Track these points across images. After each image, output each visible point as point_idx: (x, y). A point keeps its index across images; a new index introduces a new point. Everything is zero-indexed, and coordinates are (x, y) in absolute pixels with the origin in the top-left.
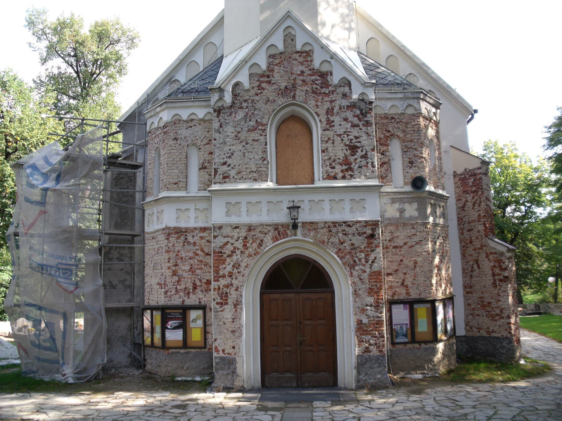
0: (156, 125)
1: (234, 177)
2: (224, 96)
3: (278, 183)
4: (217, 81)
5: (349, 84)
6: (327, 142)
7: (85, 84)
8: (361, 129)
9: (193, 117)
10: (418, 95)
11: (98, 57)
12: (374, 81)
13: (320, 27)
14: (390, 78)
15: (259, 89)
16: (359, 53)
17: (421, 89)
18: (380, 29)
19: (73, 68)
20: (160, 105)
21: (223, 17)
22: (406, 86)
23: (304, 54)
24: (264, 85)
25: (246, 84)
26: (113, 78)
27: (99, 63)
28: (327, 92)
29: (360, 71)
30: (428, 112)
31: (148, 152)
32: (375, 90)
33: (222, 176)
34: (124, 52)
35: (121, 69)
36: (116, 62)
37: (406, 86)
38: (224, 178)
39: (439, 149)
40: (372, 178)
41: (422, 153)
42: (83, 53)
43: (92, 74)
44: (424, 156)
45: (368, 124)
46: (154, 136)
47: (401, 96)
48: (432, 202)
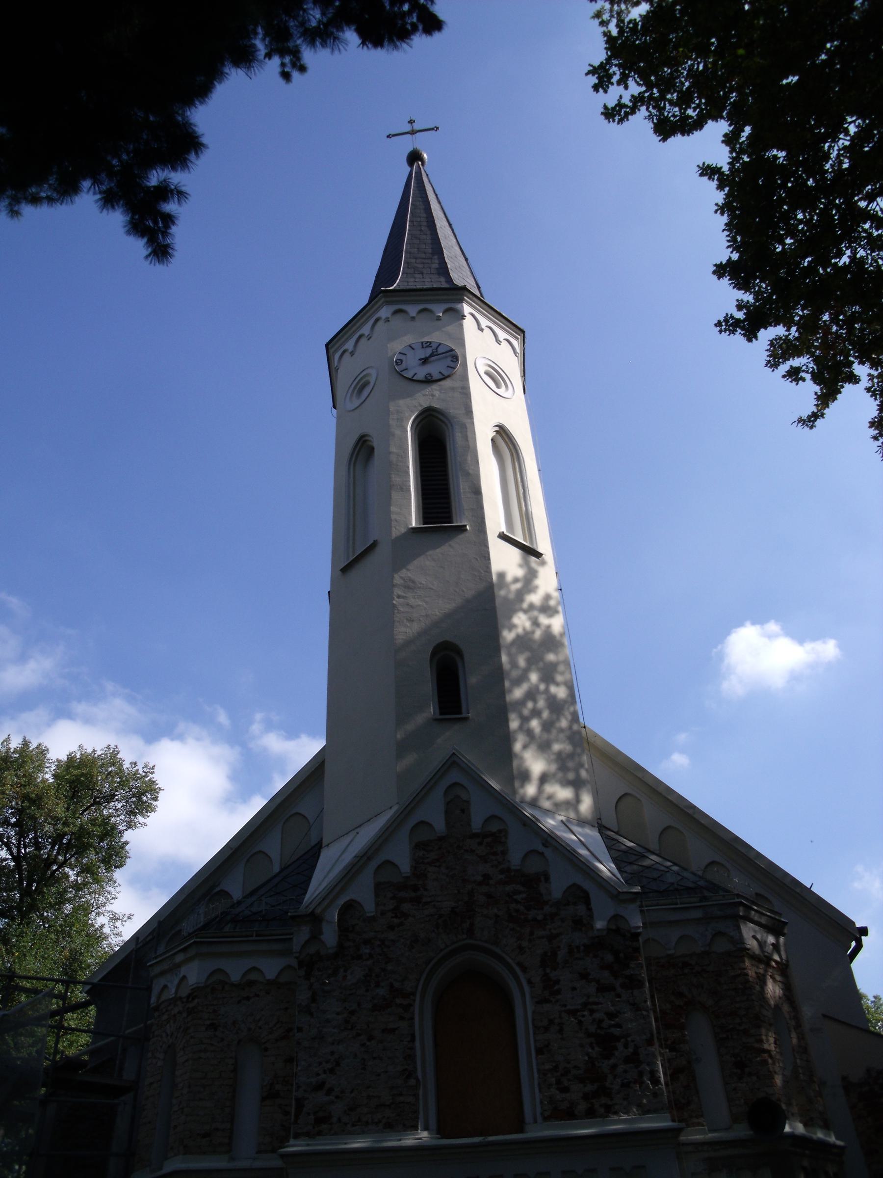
0: (171, 992)
1: (339, 1120)
2: (321, 933)
3: (441, 1131)
4: (308, 897)
5: (585, 898)
6: (546, 1029)
7: (30, 885)
8: (619, 996)
9: (253, 976)
10: (734, 911)
11: (66, 829)
12: (638, 889)
13: (517, 784)
14: (670, 878)
15: (396, 917)
16: (602, 829)
17: (738, 896)
18: (640, 775)
19: (9, 849)
20: (184, 950)
21: (323, 762)
22: (706, 894)
23: (489, 840)
24: (406, 907)
25: (369, 906)
26: (92, 874)
27: (65, 841)
28: (540, 917)
29: (606, 868)
30: (762, 944)
31: (150, 1055)
32: (641, 906)
33: (312, 1117)
34: (119, 820)
35: (111, 856)
36: (102, 839)
37: (706, 894)
38: (319, 1121)
39: (798, 1026)
40: (656, 1111)
41: (761, 1041)
42: (34, 818)
43: (49, 862)
44: (766, 1046)
45: (633, 983)
46: (165, 1017)
47: (698, 914)
48: (806, 1163)
